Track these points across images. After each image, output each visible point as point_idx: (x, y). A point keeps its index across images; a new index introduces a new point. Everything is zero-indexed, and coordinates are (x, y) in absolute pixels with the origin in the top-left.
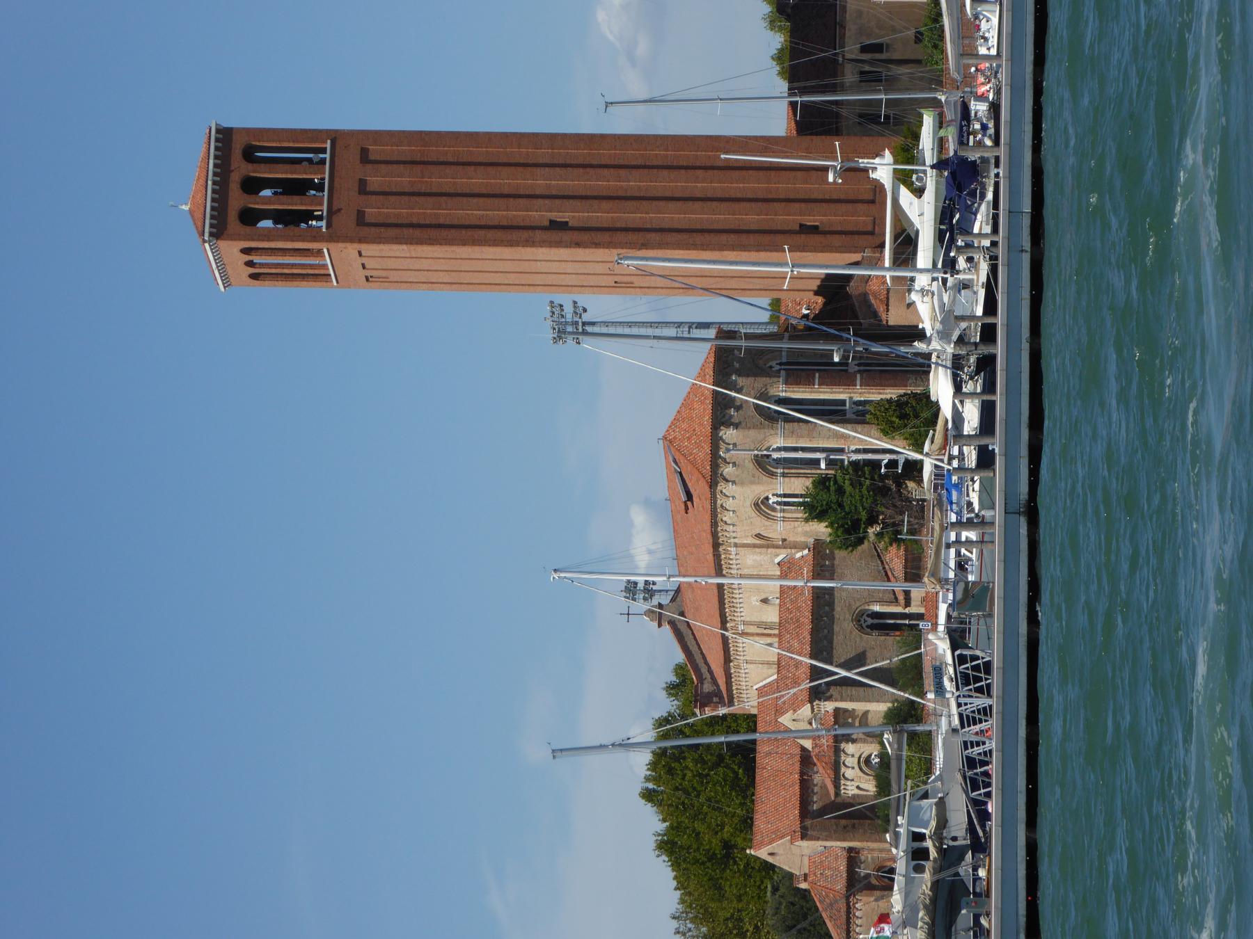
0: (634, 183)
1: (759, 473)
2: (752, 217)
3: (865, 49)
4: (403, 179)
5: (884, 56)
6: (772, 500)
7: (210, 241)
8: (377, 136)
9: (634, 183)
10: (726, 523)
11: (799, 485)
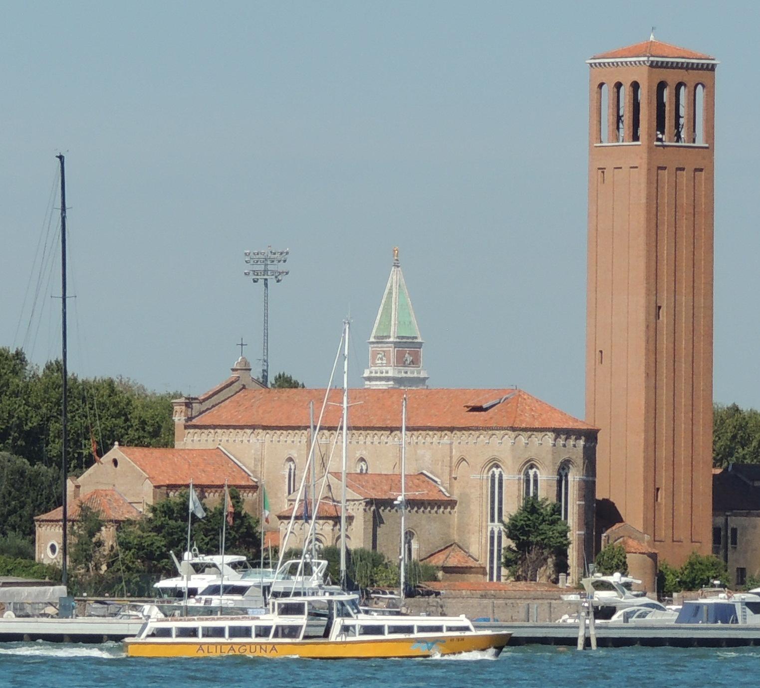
0: (684, 367)
1: (522, 461)
2: (663, 453)
3: (734, 531)
4: (685, 200)
5: (729, 545)
7: (648, 61)
8: (710, 180)
9: (684, 367)
10: (478, 437)
11: (546, 492)
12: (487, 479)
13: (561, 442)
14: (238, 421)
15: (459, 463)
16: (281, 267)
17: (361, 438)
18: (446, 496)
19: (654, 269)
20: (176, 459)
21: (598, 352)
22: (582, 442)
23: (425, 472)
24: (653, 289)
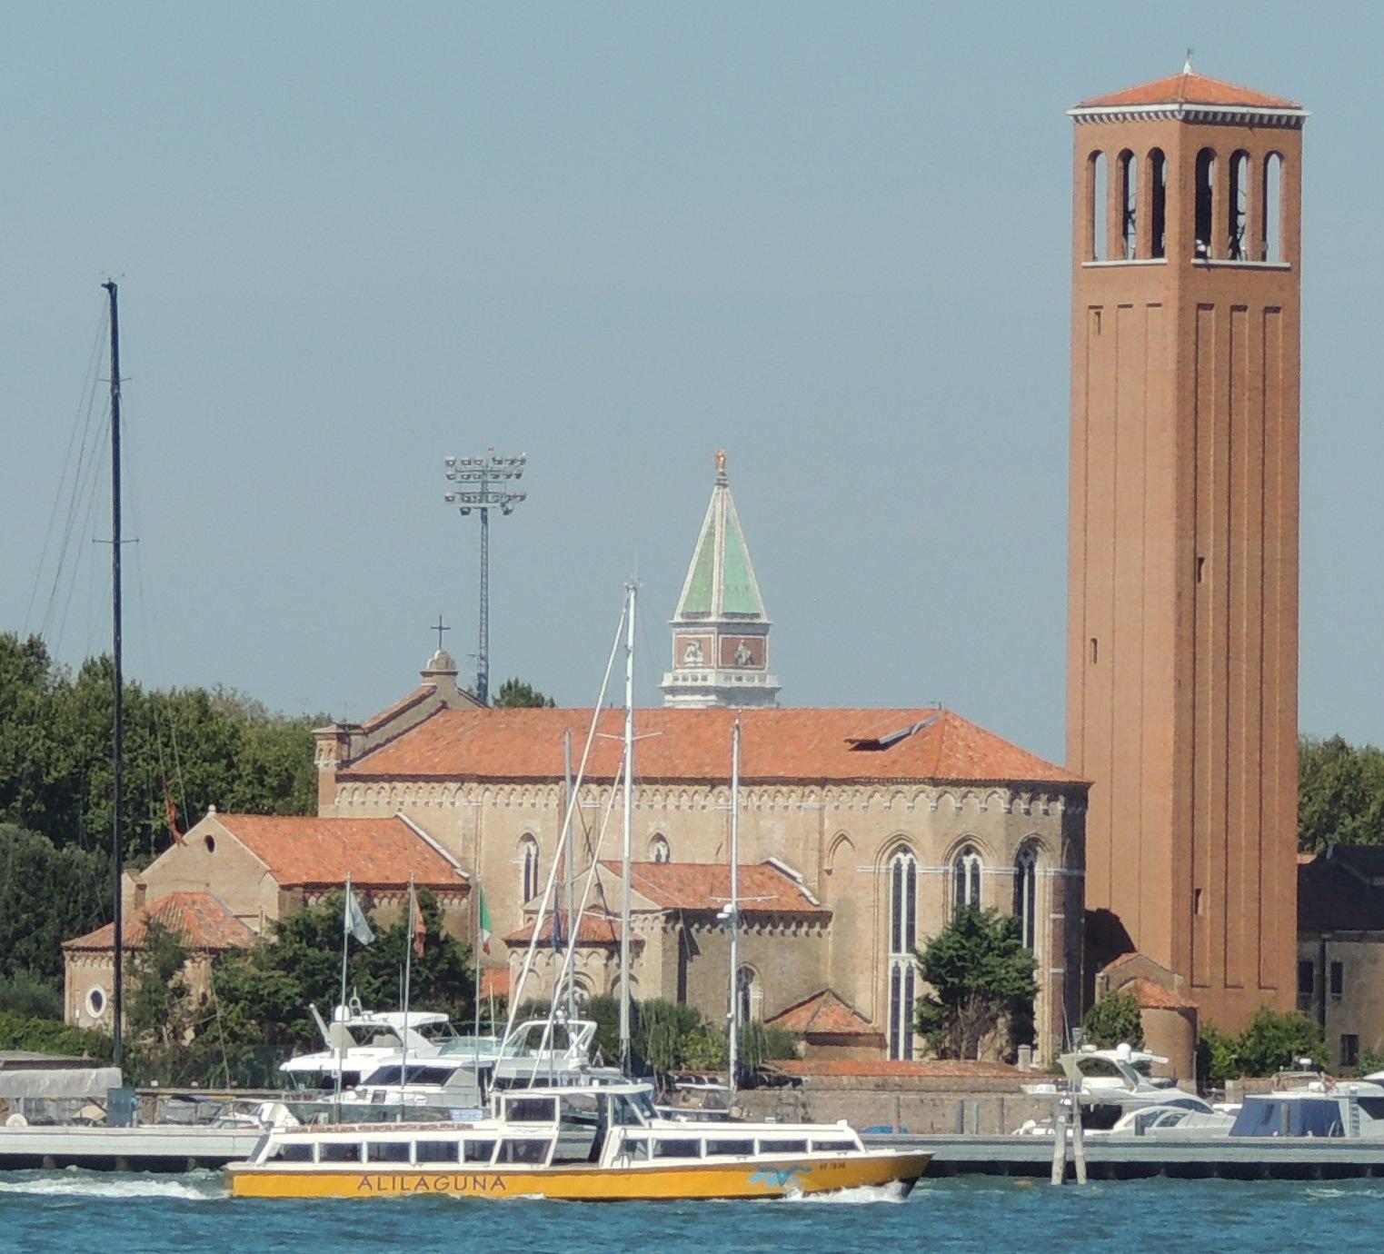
0: (1245, 670)
1: (951, 841)
2: (1208, 825)
3: (1337, 968)
4: (1247, 364)
5: (1328, 994)
7: (1180, 111)
8: (1294, 327)
9: (1245, 670)
10: (871, 797)
11: (994, 897)
12: (888, 874)
13: (1021, 805)
14: (434, 767)
15: (836, 843)
16: (512, 487)
17: (658, 798)
18: (812, 903)
20: (320, 837)
21: (1088, 642)
23: (773, 860)
24: (1190, 526)
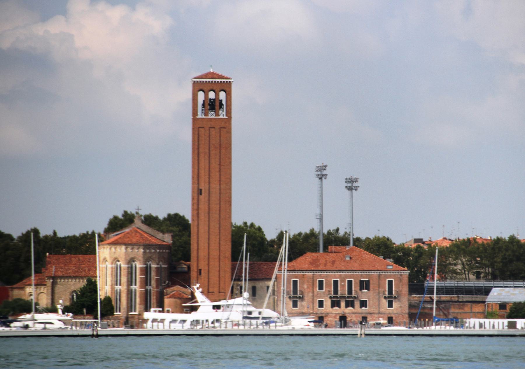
1: (128, 258)
6: (118, 263)
19: (196, 173)
22: (142, 250)
24: (196, 182)
